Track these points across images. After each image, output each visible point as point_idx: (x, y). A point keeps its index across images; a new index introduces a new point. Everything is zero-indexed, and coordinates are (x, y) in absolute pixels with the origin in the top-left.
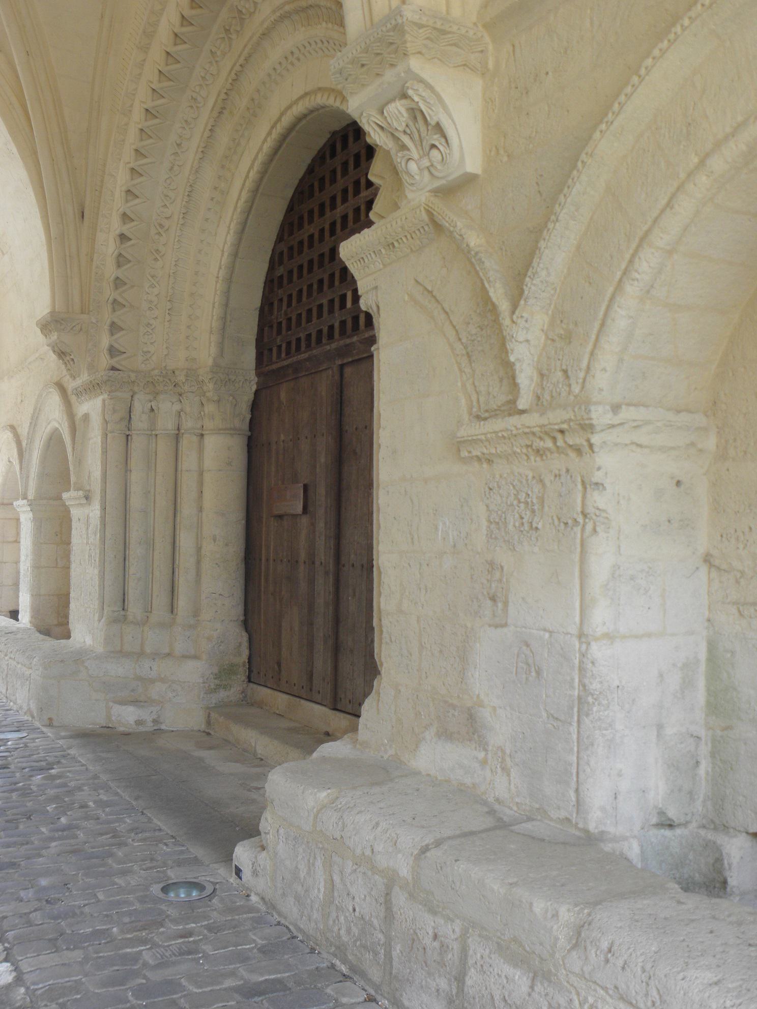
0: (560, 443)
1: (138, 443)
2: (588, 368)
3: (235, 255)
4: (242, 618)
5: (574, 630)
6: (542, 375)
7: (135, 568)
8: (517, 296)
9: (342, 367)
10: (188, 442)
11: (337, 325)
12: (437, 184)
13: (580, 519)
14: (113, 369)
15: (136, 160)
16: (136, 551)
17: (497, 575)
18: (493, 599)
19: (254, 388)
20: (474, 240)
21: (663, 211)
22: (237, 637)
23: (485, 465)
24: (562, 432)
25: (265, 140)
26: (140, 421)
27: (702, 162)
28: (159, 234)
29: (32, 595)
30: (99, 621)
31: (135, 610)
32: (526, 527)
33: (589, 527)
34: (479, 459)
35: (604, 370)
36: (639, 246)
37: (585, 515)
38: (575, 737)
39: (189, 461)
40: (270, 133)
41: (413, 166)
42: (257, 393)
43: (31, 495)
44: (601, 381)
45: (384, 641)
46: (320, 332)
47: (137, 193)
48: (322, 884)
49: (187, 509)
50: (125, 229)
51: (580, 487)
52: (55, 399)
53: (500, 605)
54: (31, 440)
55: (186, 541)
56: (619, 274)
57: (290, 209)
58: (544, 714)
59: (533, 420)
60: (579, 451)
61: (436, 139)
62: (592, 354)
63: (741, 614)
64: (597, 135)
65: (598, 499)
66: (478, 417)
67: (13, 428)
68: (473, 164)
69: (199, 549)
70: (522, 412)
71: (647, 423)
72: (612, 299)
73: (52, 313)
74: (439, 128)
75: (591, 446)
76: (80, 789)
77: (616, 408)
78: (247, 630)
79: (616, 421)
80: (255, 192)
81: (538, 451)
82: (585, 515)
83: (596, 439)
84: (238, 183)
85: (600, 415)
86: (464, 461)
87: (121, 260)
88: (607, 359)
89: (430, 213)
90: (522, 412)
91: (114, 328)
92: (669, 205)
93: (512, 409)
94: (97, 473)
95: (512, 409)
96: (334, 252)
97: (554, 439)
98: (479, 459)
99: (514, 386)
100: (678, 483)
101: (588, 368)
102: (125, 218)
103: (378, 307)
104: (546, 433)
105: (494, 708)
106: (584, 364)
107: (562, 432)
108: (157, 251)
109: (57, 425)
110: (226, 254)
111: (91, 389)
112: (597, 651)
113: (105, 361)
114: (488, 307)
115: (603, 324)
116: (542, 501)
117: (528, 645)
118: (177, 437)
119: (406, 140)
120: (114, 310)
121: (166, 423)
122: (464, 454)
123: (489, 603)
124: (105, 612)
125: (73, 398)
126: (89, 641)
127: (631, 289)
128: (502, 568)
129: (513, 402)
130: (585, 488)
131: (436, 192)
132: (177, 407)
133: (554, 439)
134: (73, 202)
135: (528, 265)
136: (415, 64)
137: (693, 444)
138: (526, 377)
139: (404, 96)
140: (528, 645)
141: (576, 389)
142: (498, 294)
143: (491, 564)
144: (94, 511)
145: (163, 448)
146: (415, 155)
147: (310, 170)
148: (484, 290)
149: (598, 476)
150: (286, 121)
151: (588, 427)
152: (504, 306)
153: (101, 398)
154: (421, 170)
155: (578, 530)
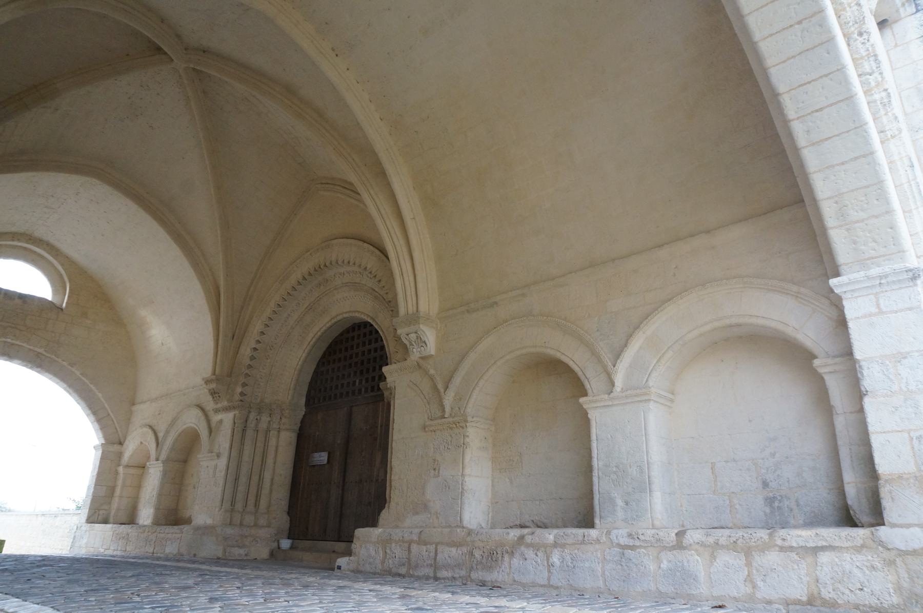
0: (458, 425)
1: (250, 433)
2: (466, 407)
3: (305, 361)
4: (287, 510)
5: (460, 474)
6: (452, 409)
7: (241, 488)
8: (446, 388)
9: (352, 407)
10: (273, 433)
11: (333, 395)
12: (421, 356)
13: (463, 445)
14: (241, 401)
15: (268, 321)
16: (243, 480)
17: (436, 463)
18: (435, 469)
19: (304, 413)
20: (432, 372)
21: (485, 372)
22: (286, 518)
23: (433, 433)
24: (459, 423)
25: (328, 322)
26: (251, 424)
27: (495, 362)
28: (271, 349)
29: (155, 509)
30: (219, 511)
31: (239, 506)
32: (446, 448)
33: (465, 447)
34: (431, 431)
35: (470, 408)
36: (479, 379)
37: (464, 444)
38: (460, 502)
39: (273, 442)
40: (330, 320)
41: (415, 350)
42: (304, 416)
43: (163, 456)
44: (469, 410)
45: (392, 489)
46: (336, 395)
47: (265, 333)
48: (381, 554)
49: (270, 461)
50: (258, 346)
51: (463, 437)
52: (197, 412)
53: (437, 471)
54: (165, 437)
55: (267, 476)
56: (474, 385)
57: (330, 346)
58: (450, 499)
59: (451, 420)
60: (463, 428)
61: (423, 345)
62: (467, 404)
63: (500, 472)
64: (470, 352)
65: (467, 440)
66: (431, 420)
67: (151, 427)
68: (433, 353)
69: (272, 480)
70: (446, 418)
71: (480, 422)
72: (473, 390)
73: (214, 374)
74: (425, 342)
75: (466, 426)
76: (433, 444)
77: (473, 417)
78: (289, 516)
79: (472, 420)
80: (318, 339)
81: (451, 428)
82: (464, 444)
83: (468, 424)
84: (311, 335)
85: (469, 419)
86: (426, 432)
87: (252, 358)
88: (470, 405)
89: (418, 363)
90: (446, 418)
91: (244, 385)
92: (487, 370)
93: (443, 417)
94: (227, 445)
95: (443, 417)
96: (381, 369)
97: (456, 425)
98: (431, 431)
99: (444, 411)
100: (485, 438)
101: (466, 407)
102: (258, 342)
103: (395, 387)
104: (454, 423)
105: (434, 501)
106: (465, 406)
107: (459, 423)
108: (269, 356)
109: (193, 425)
110: (301, 360)
111: (227, 409)
112: (467, 479)
113: (237, 397)
114: (437, 390)
115: (470, 396)
116: (451, 442)
117: (446, 481)
118: (268, 431)
119: (413, 343)
120: (245, 378)
121: (263, 425)
122: (427, 429)
123: (433, 471)
124: (223, 507)
125: (211, 414)
126: (209, 521)
127: (477, 389)
128: (438, 461)
129: (444, 415)
130: (464, 437)
131: (420, 358)
132: (269, 419)
133: (456, 425)
134: (632, 402)
135: (450, 380)
136: (421, 326)
137: (489, 429)
138: (448, 409)
139: (416, 333)
140: (446, 481)
141: (462, 412)
142: (440, 387)
143: (435, 460)
144: (223, 462)
145: (261, 437)
146: (416, 347)
147: (342, 334)
148: (436, 386)
149: (468, 434)
150: (339, 318)
151: (466, 421)
152: (442, 390)
153: (234, 413)
154: (417, 351)
155: (462, 448)
